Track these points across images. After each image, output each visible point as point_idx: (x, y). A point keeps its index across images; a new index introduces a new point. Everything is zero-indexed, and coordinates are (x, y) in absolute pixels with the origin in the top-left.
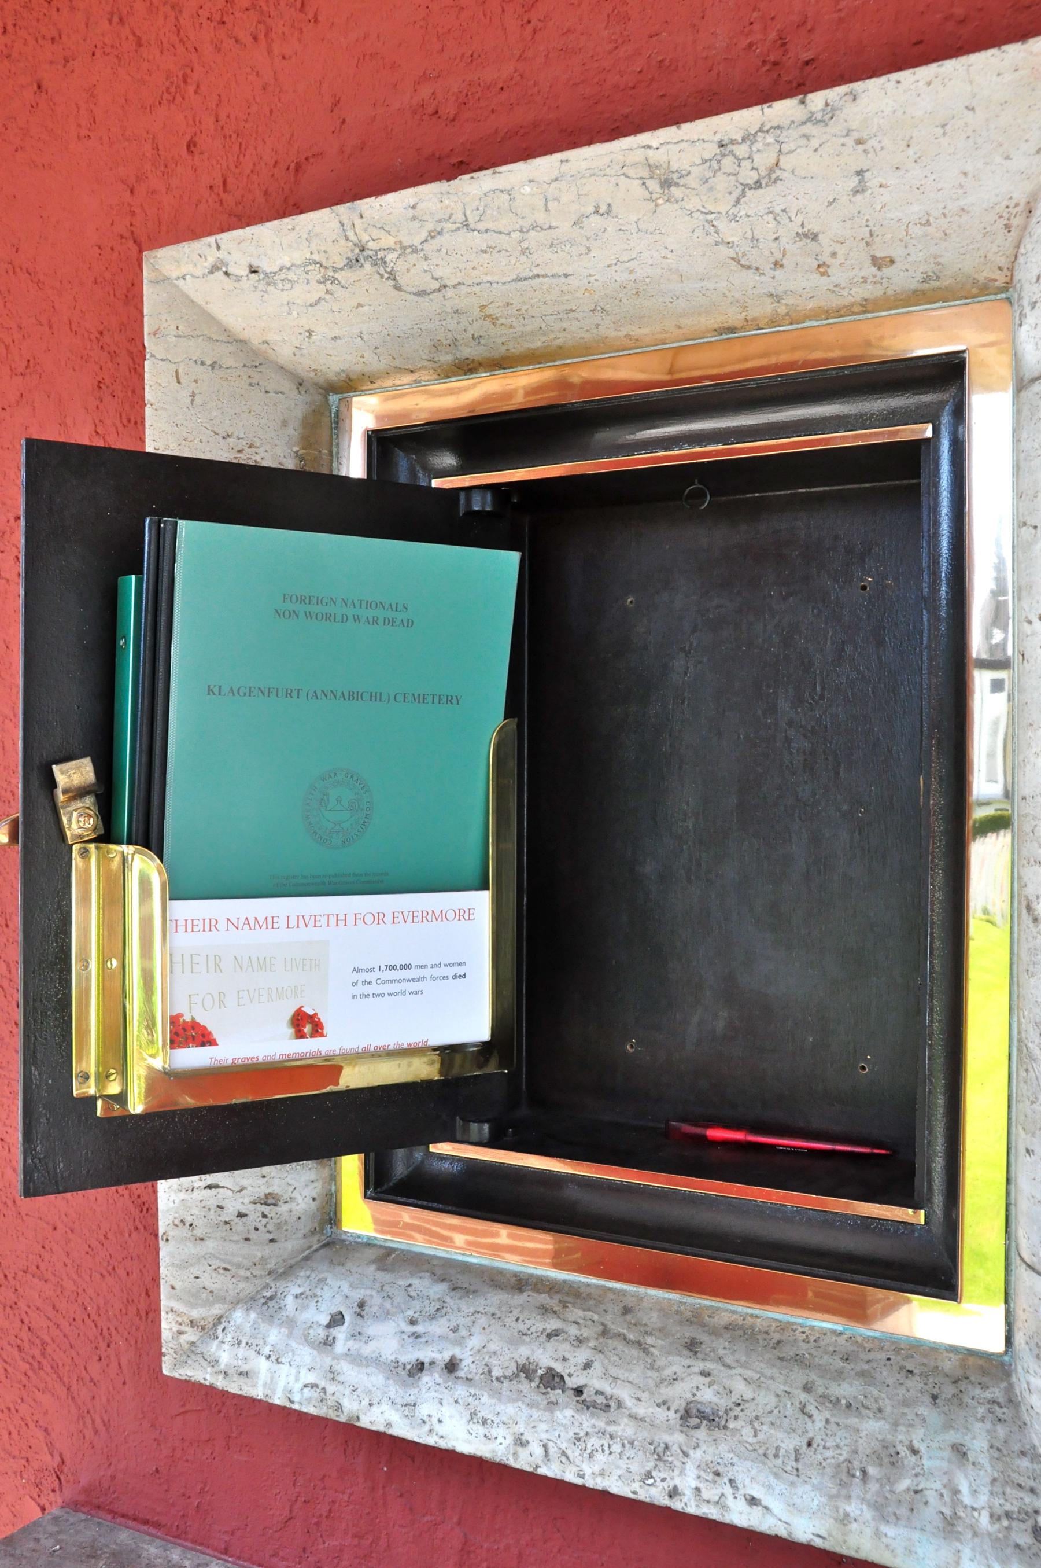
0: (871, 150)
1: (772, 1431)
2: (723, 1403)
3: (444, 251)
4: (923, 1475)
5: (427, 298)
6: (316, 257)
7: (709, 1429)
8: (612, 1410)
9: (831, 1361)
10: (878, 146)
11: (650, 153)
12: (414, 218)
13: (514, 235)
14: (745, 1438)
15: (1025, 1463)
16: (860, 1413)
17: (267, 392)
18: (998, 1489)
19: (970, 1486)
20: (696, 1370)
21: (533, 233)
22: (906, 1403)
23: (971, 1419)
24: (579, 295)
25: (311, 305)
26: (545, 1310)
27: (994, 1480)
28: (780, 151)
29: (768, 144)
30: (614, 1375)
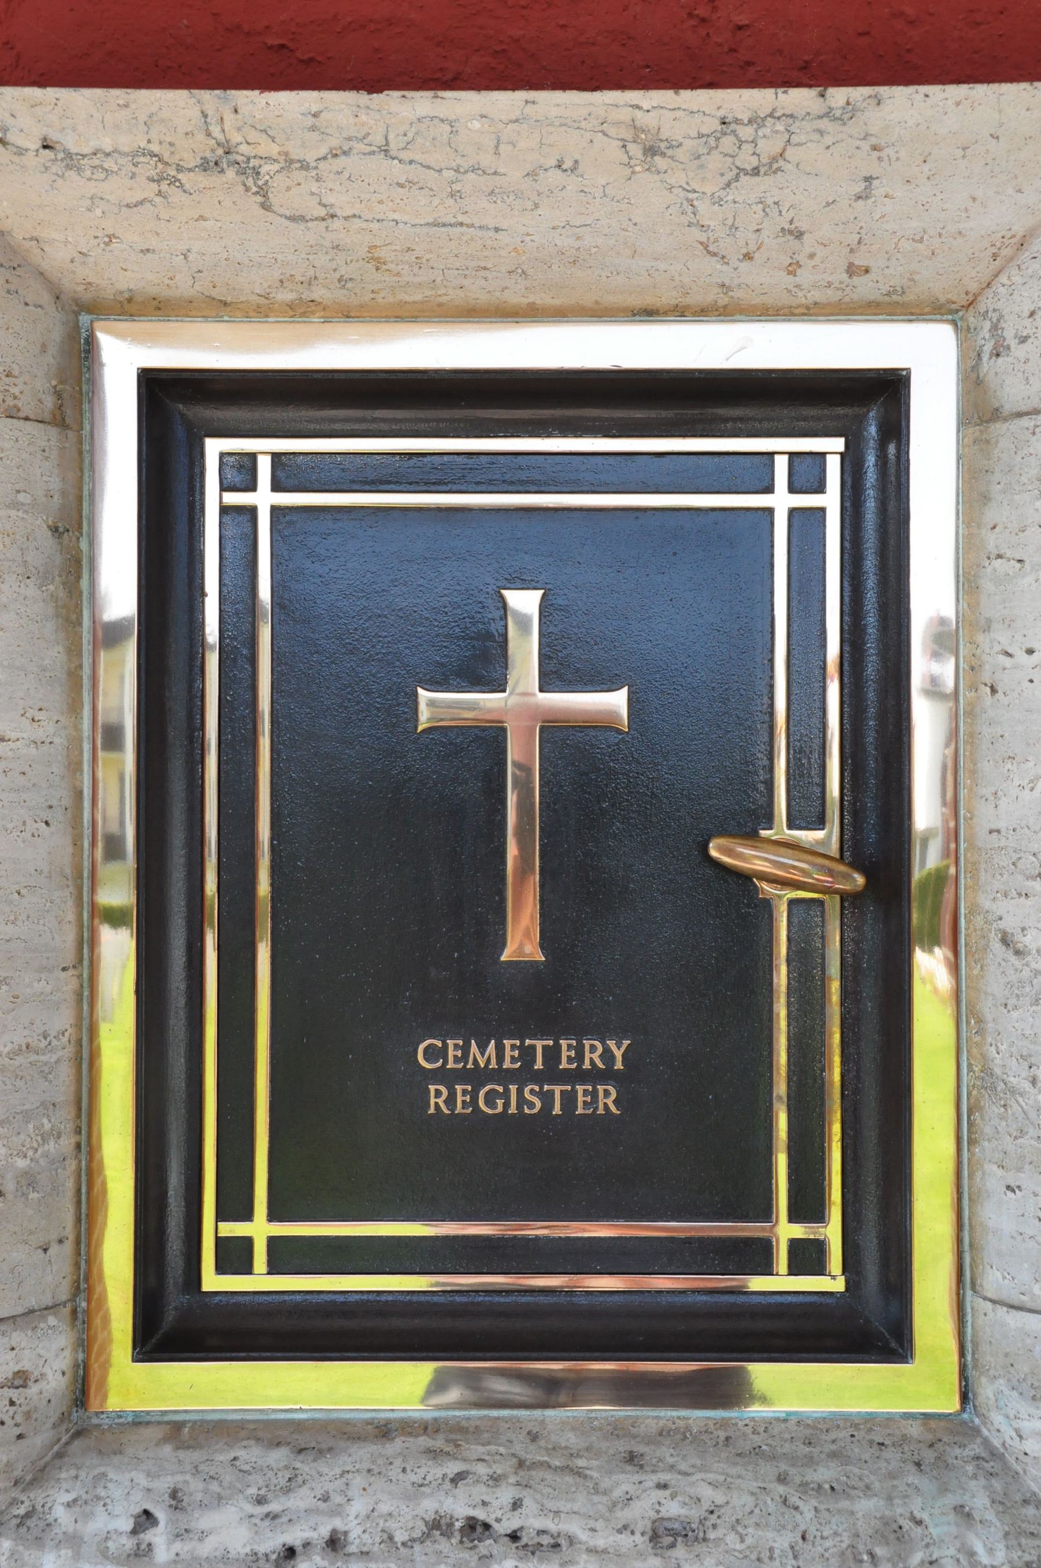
0: (886, 159)
1: (760, 1533)
2: (694, 1514)
3: (346, 175)
4: (934, 1544)
5: (302, 226)
6: (155, 148)
7: (686, 1545)
8: (564, 1549)
9: (794, 1448)
10: (894, 157)
11: (639, 114)
12: (313, 128)
13: (445, 173)
14: (731, 1546)
15: (1030, 1511)
16: (849, 1495)
17: (26, 304)
18: (1013, 1542)
19: (985, 1545)
20: (650, 1484)
21: (471, 176)
22: (892, 1476)
23: (964, 1479)
24: (503, 253)
25: (128, 206)
26: (433, 1454)
27: (1006, 1535)
28: (789, 141)
29: (777, 132)
30: (555, 1509)
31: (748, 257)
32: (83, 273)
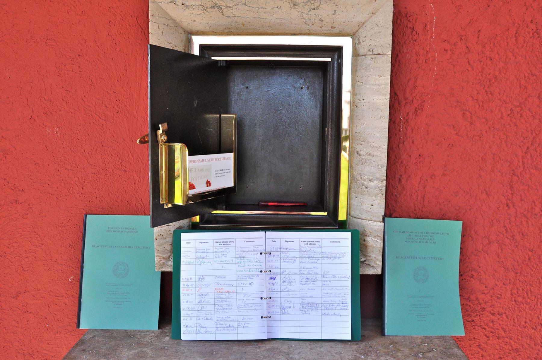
31: (313, 24)
32: (189, 27)
